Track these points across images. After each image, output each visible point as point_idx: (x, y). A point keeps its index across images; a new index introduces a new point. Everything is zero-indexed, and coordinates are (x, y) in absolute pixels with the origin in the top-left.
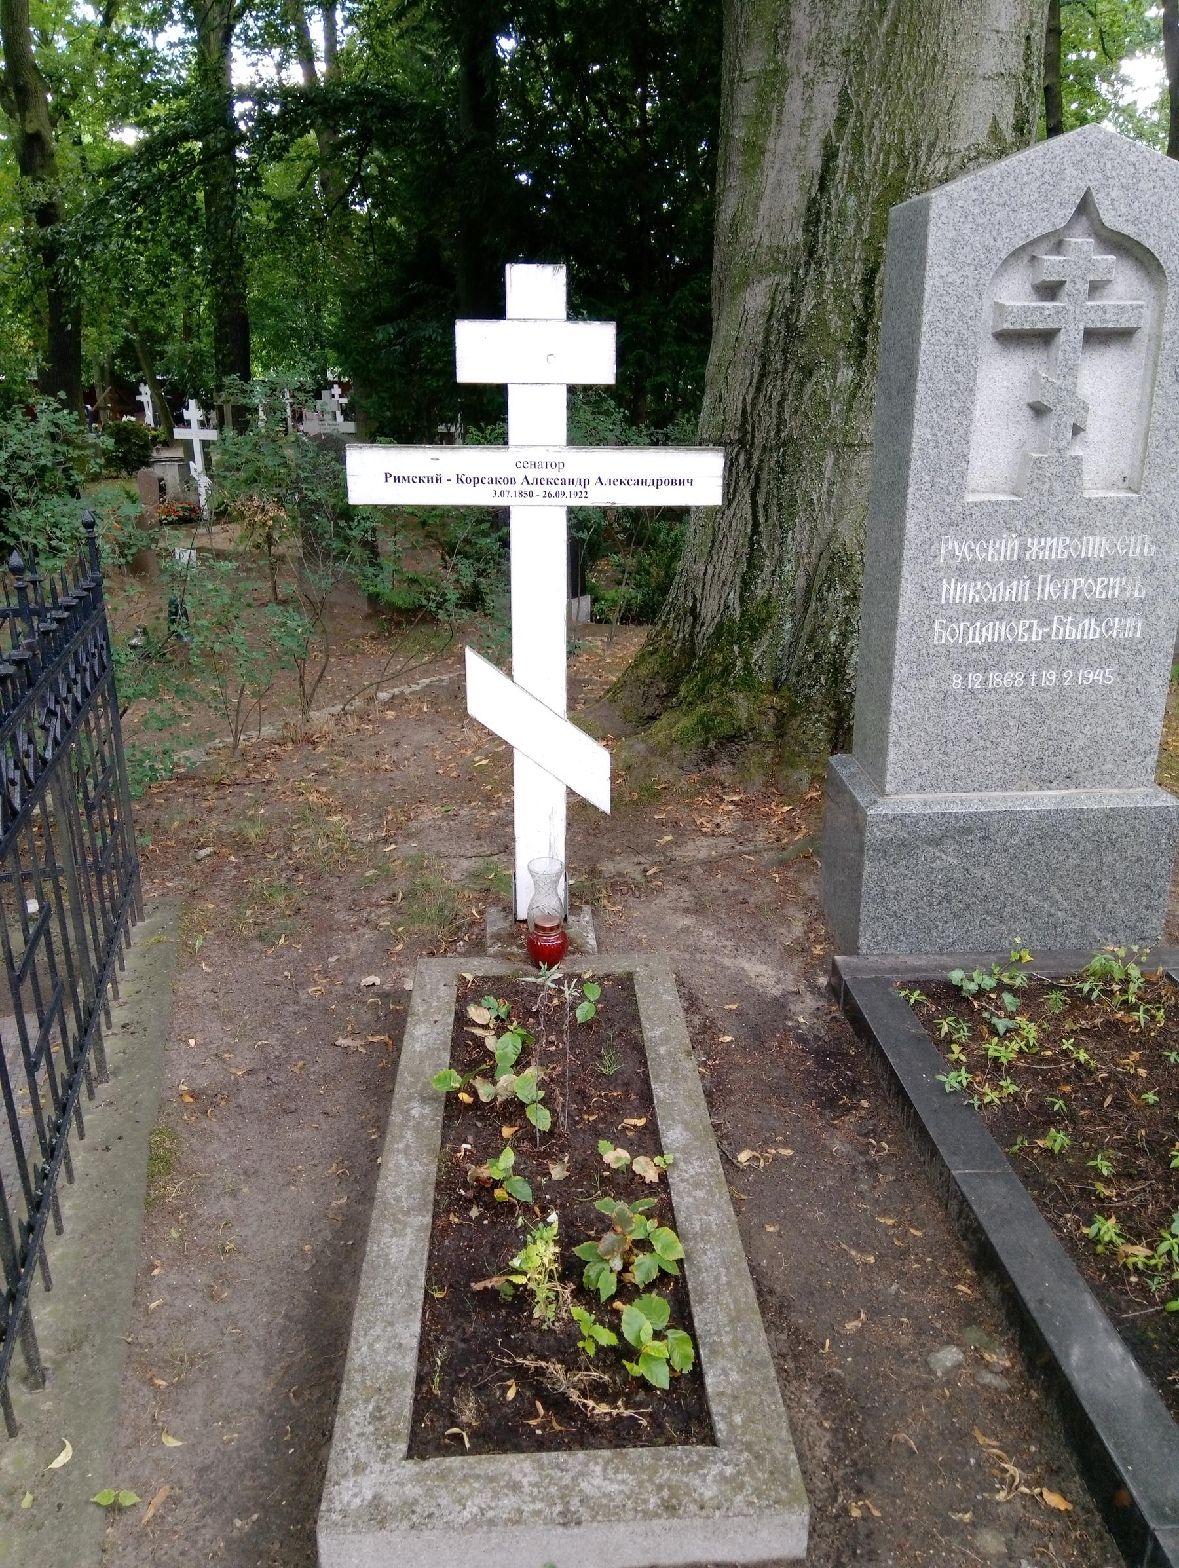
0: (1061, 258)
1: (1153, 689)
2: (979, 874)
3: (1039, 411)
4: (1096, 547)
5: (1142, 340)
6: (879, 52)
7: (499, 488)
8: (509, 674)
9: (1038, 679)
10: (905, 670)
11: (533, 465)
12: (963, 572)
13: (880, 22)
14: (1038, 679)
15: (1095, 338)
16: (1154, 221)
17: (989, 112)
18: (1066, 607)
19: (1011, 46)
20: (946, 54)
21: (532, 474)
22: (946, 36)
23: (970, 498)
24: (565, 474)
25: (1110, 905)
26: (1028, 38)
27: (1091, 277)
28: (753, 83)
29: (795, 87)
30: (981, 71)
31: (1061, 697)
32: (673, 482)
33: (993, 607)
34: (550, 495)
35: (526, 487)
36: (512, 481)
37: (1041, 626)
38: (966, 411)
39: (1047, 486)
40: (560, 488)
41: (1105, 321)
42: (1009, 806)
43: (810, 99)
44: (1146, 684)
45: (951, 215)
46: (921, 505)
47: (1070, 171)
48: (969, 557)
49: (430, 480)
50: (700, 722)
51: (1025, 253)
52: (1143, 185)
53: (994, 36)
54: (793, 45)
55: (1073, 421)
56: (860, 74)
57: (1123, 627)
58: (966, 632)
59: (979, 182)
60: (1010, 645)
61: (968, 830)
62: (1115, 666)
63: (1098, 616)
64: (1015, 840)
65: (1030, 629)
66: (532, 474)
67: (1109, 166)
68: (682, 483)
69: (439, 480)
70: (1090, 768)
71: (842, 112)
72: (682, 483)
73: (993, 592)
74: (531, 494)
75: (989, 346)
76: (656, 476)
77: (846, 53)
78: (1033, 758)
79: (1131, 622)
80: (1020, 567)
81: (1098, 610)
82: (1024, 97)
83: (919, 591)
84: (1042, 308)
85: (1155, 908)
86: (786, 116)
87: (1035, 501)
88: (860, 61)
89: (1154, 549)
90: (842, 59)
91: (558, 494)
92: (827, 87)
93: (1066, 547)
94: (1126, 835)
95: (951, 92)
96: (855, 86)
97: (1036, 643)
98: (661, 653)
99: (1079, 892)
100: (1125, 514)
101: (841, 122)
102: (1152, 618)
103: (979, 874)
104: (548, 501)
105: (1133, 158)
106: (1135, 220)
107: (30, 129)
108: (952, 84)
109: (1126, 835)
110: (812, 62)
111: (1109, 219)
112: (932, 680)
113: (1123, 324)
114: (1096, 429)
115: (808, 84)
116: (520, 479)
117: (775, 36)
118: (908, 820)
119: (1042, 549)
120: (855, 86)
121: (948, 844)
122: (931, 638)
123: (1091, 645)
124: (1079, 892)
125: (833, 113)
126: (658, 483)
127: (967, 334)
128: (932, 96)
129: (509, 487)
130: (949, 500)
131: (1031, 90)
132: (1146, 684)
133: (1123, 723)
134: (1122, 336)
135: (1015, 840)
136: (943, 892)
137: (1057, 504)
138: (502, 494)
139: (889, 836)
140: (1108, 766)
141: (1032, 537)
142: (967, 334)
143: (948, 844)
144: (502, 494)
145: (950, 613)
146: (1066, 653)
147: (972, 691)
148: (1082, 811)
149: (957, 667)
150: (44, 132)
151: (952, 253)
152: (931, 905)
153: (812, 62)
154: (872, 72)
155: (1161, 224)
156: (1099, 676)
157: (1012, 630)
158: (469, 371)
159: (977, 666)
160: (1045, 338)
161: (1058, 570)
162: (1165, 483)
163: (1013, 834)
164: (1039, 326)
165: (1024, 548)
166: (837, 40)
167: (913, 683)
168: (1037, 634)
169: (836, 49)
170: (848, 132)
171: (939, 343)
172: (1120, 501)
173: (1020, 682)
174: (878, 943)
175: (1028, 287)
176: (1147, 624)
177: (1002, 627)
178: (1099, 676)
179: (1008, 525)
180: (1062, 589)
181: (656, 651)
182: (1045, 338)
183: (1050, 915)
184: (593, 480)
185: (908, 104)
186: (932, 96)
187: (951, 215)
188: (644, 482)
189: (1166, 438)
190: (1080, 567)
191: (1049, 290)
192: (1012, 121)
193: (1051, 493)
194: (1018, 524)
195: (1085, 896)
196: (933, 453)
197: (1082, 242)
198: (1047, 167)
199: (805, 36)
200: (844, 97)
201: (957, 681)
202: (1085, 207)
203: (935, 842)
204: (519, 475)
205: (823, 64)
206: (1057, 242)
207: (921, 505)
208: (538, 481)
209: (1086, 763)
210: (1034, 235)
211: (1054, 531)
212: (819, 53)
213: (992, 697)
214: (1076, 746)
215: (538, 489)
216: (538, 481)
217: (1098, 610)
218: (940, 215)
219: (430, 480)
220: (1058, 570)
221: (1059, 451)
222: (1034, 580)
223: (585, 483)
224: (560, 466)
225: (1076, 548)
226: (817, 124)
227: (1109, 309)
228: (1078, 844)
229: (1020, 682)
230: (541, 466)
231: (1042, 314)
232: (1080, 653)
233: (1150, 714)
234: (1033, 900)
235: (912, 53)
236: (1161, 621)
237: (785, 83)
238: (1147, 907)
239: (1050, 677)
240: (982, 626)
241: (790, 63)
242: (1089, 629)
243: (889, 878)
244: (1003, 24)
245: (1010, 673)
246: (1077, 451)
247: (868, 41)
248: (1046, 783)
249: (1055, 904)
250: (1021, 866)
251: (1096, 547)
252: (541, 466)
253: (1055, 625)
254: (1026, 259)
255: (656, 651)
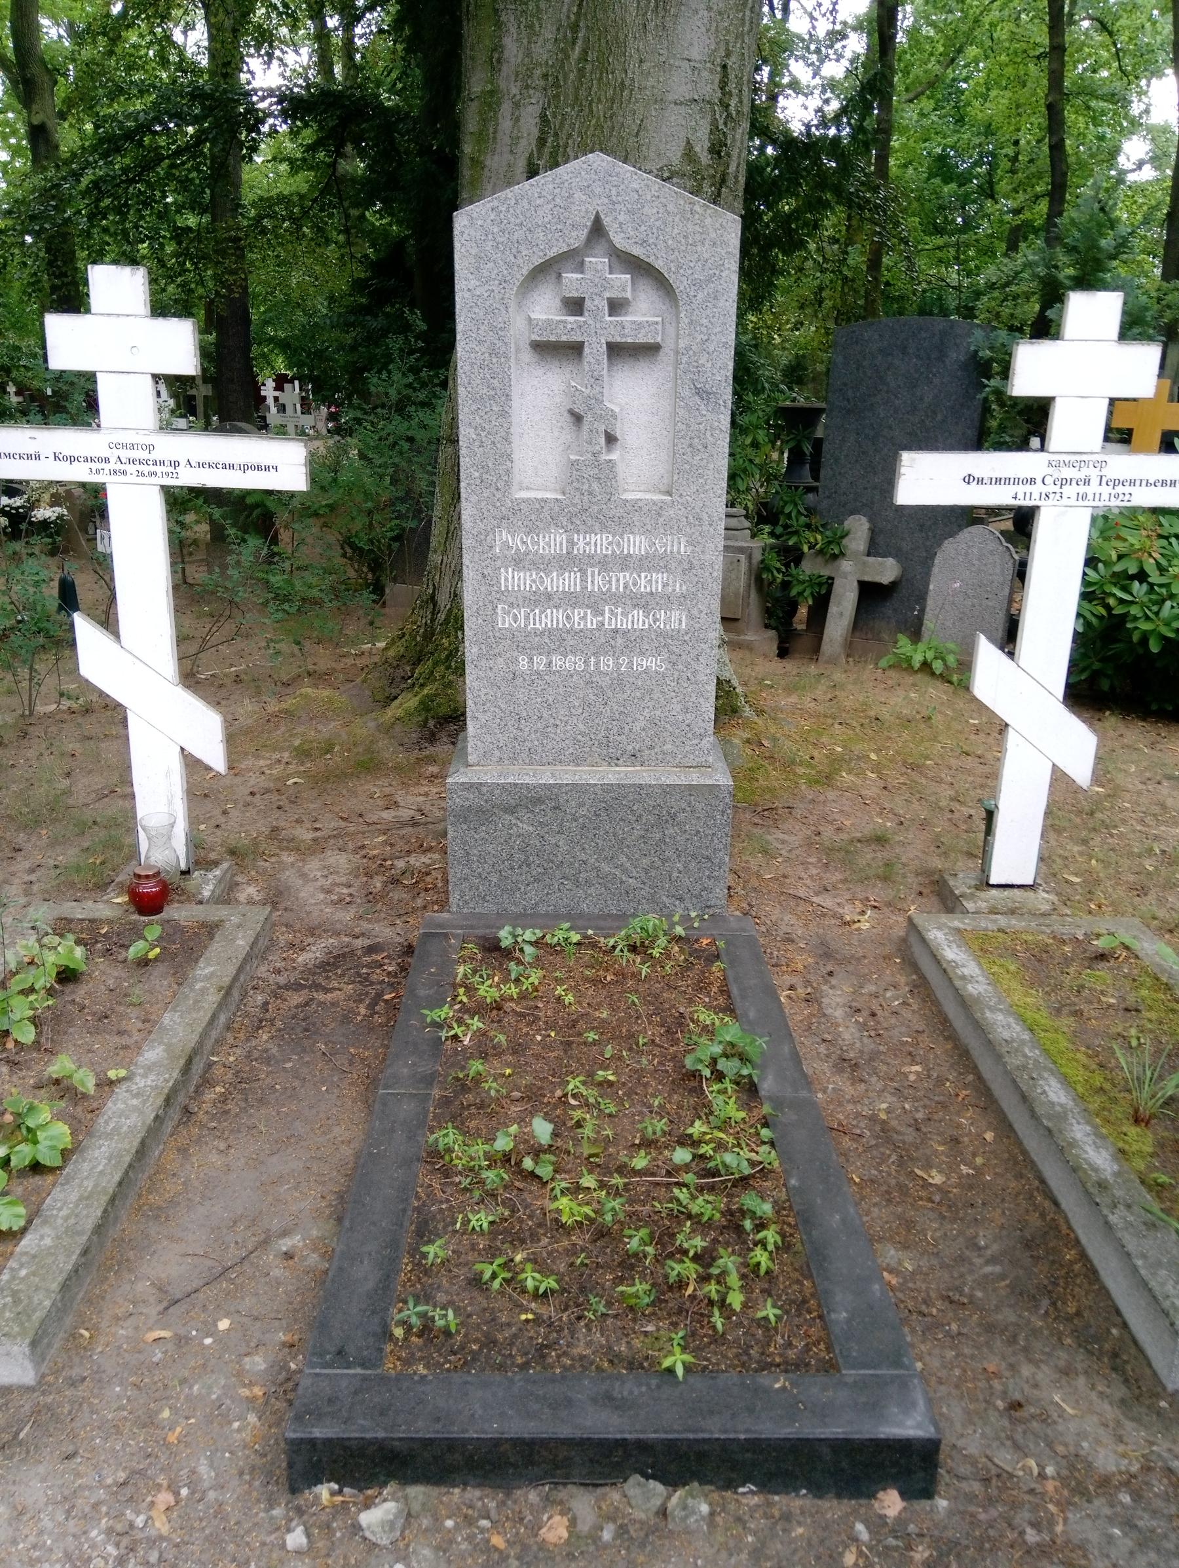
0: (579, 276)
1: (702, 677)
2: (553, 841)
3: (577, 418)
4: (636, 544)
5: (666, 355)
6: (572, 76)
7: (94, 466)
8: (116, 635)
9: (597, 663)
10: (475, 650)
11: (125, 446)
12: (519, 562)
13: (573, 49)
14: (597, 663)
15: (617, 351)
16: (661, 245)
17: (682, 135)
18: (616, 599)
19: (705, 74)
20: (633, 80)
21: (125, 454)
22: (633, 65)
23: (523, 494)
24: (156, 455)
25: (675, 874)
26: (724, 67)
27: (607, 295)
28: (476, 103)
29: (506, 108)
30: (670, 97)
31: (619, 681)
32: (259, 468)
33: (549, 596)
34: (143, 474)
35: (119, 466)
36: (107, 460)
37: (595, 616)
38: (504, 414)
39: (586, 487)
40: (153, 468)
41: (624, 336)
42: (577, 779)
43: (517, 120)
44: (695, 672)
45: (473, 233)
46: (474, 498)
47: (578, 195)
48: (523, 549)
49: (29, 457)
50: (422, 702)
51: (547, 270)
52: (646, 210)
53: (685, 64)
54: (505, 68)
55: (603, 428)
56: (556, 97)
57: (668, 620)
58: (527, 617)
59: (496, 203)
60: (568, 632)
61: (538, 801)
62: (665, 654)
63: (645, 607)
64: (583, 811)
65: (584, 618)
66: (125, 454)
67: (614, 192)
68: (267, 468)
69: (38, 457)
70: (652, 748)
71: (542, 132)
72: (267, 468)
73: (547, 582)
74: (125, 473)
75: (527, 356)
76: (242, 461)
77: (545, 76)
78: (600, 737)
79: (675, 615)
80: (569, 561)
81: (645, 603)
82: (721, 122)
83: (480, 577)
84: (565, 322)
85: (716, 878)
86: (499, 135)
87: (576, 500)
88: (556, 85)
89: (689, 549)
90: (542, 83)
91: (151, 474)
92: (530, 108)
93: (610, 543)
94: (684, 810)
95: (639, 116)
96: (552, 109)
97: (591, 631)
98: (407, 637)
99: (646, 861)
100: (660, 515)
101: (542, 141)
102: (695, 612)
103: (553, 841)
104: (141, 480)
105: (635, 185)
106: (644, 243)
107: (36, 121)
108: (639, 107)
109: (684, 810)
110: (519, 84)
111: (619, 241)
112: (500, 660)
113: (641, 338)
114: (629, 433)
115: (517, 105)
116: (113, 460)
117: (491, 59)
118: (484, 789)
119: (588, 544)
120: (552, 109)
121: (522, 812)
122: (495, 621)
123: (642, 636)
124: (646, 861)
125: (536, 132)
126: (245, 468)
127: (499, 344)
128: (621, 119)
129: (103, 465)
130: (499, 495)
131: (729, 116)
132: (695, 672)
133: (678, 707)
134: (647, 350)
135: (583, 811)
136: (523, 857)
137: (598, 503)
138: (98, 472)
139: (468, 803)
140: (668, 747)
141: (578, 532)
142: (499, 344)
143: (522, 812)
144: (98, 472)
145: (511, 600)
146: (620, 641)
147: (538, 673)
148: (641, 786)
149: (522, 650)
150: (49, 124)
151: (477, 268)
152: (512, 868)
153: (519, 84)
154: (567, 95)
155: (667, 247)
156: (652, 663)
157: (568, 617)
158: (1148, 355)
159: (540, 650)
160: (574, 350)
161: (604, 564)
162: (694, 488)
163: (581, 805)
164: (564, 338)
165: (572, 543)
166: (538, 64)
167: (483, 662)
168: (592, 622)
169: (538, 72)
170: (547, 150)
171: (472, 350)
172: (654, 503)
173: (580, 666)
174: (467, 903)
175: (557, 303)
176: (691, 617)
177: (559, 614)
178: (652, 663)
179: (554, 520)
180: (610, 582)
181: (404, 635)
182: (574, 350)
183: (622, 882)
184: (183, 462)
185: (599, 127)
186: (621, 119)
187: (473, 233)
188: (232, 466)
189: (690, 445)
190: (625, 562)
191: (575, 306)
192: (707, 144)
193: (590, 493)
194: (564, 521)
195: (652, 865)
196: (479, 451)
197: (598, 261)
198: (557, 191)
199: (513, 60)
200: (543, 117)
201: (523, 662)
202: (598, 229)
203: (511, 810)
204: (113, 454)
205: (527, 87)
206: (572, 258)
207: (474, 498)
208: (131, 461)
209: (648, 742)
210: (552, 253)
211: (597, 527)
212: (524, 76)
213: (557, 678)
214: (637, 727)
215: (131, 469)
216: (131, 461)
217: (645, 603)
218: (462, 233)
219: (29, 457)
220: (604, 564)
221: (594, 454)
222: (583, 573)
223: (176, 464)
224: (150, 447)
225: (618, 544)
226: (523, 142)
227: (627, 325)
228: (640, 816)
229: (580, 666)
230: (132, 447)
231: (568, 327)
232: (632, 642)
233: (701, 700)
234: (606, 868)
235: (601, 78)
236: (703, 615)
237: (499, 104)
238: (709, 878)
239: (607, 663)
240: (541, 613)
241: (502, 84)
242: (637, 620)
243: (471, 842)
244: (696, 53)
245: (571, 657)
246: (614, 456)
247: (562, 67)
248: (613, 760)
249: (625, 871)
250: (590, 836)
251: (636, 544)
252: (132, 447)
253: (607, 615)
254: (554, 276)
255: (404, 635)
